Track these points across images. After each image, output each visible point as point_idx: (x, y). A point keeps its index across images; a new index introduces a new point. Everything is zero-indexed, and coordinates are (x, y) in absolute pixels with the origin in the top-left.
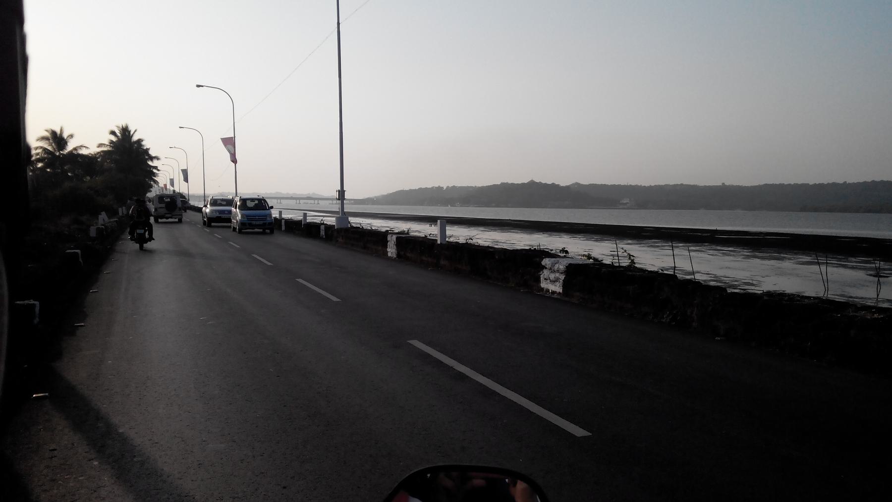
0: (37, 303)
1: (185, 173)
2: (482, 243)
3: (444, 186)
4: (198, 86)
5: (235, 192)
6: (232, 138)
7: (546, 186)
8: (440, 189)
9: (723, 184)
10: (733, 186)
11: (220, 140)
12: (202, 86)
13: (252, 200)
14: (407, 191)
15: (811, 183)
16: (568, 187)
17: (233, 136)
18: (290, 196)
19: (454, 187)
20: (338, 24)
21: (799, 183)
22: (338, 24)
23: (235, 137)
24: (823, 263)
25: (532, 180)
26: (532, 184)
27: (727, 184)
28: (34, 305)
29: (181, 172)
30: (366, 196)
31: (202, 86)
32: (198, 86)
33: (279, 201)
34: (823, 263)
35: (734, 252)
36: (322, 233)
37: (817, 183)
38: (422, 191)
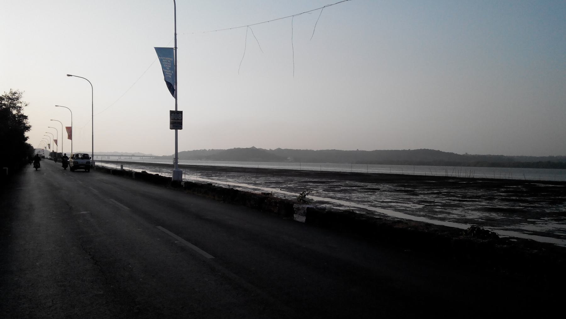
0: (7, 168)
2: (148, 173)
4: (69, 75)
5: (92, 152)
8: (205, 150)
12: (71, 76)
13: (81, 154)
14: (282, 149)
16: (463, 155)
17: (173, 46)
19: (213, 150)
20: (176, 34)
21: (112, 152)
22: (176, 34)
23: (176, 48)
25: (253, 147)
26: (439, 151)
28: (6, 169)
31: (71, 76)
32: (69, 75)
33: (120, 158)
35: (345, 193)
38: (484, 157)
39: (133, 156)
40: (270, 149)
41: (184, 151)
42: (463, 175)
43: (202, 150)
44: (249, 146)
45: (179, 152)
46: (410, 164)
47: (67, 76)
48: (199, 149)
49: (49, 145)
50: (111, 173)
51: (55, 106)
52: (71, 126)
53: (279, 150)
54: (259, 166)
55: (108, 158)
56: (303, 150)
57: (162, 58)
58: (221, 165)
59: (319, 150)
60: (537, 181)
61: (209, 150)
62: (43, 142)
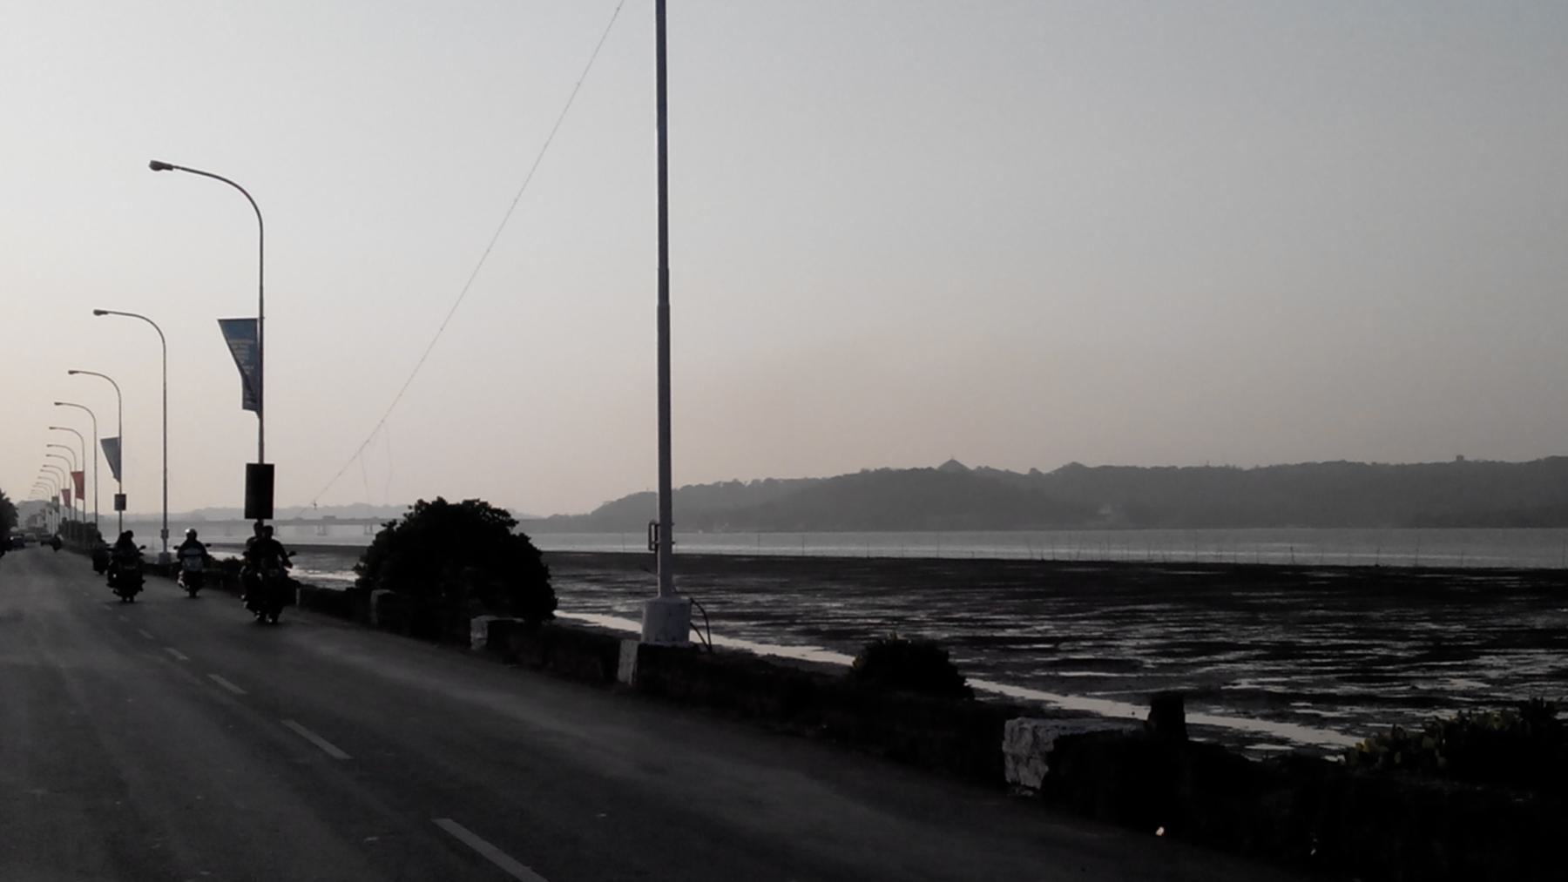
1: (113, 448)
3: (746, 479)
4: (98, 313)
6: (255, 320)
7: (901, 473)
8: (735, 485)
9: (1460, 458)
10: (1385, 466)
11: (218, 329)
12: (169, 167)
14: (708, 486)
15: (1247, 465)
18: (290, 518)
23: (262, 318)
24: (702, 627)
27: (1470, 457)
29: (99, 443)
30: (350, 517)
31: (169, 167)
34: (702, 627)
36: (627, 668)
37: (454, 498)
39: (330, 520)
40: (1033, 470)
41: (644, 490)
42: (1208, 554)
43: (726, 484)
44: (933, 460)
45: (677, 483)
46: (1442, 522)
47: (150, 169)
48: (708, 482)
49: (79, 477)
50: (374, 617)
51: (45, 457)
52: (256, 315)
53: (1074, 472)
54: (627, 547)
55: (366, 533)
56: (1189, 471)
57: (231, 342)
58: (830, 548)
59: (1264, 465)
60: (1485, 569)
61: (755, 482)
62: (57, 474)
